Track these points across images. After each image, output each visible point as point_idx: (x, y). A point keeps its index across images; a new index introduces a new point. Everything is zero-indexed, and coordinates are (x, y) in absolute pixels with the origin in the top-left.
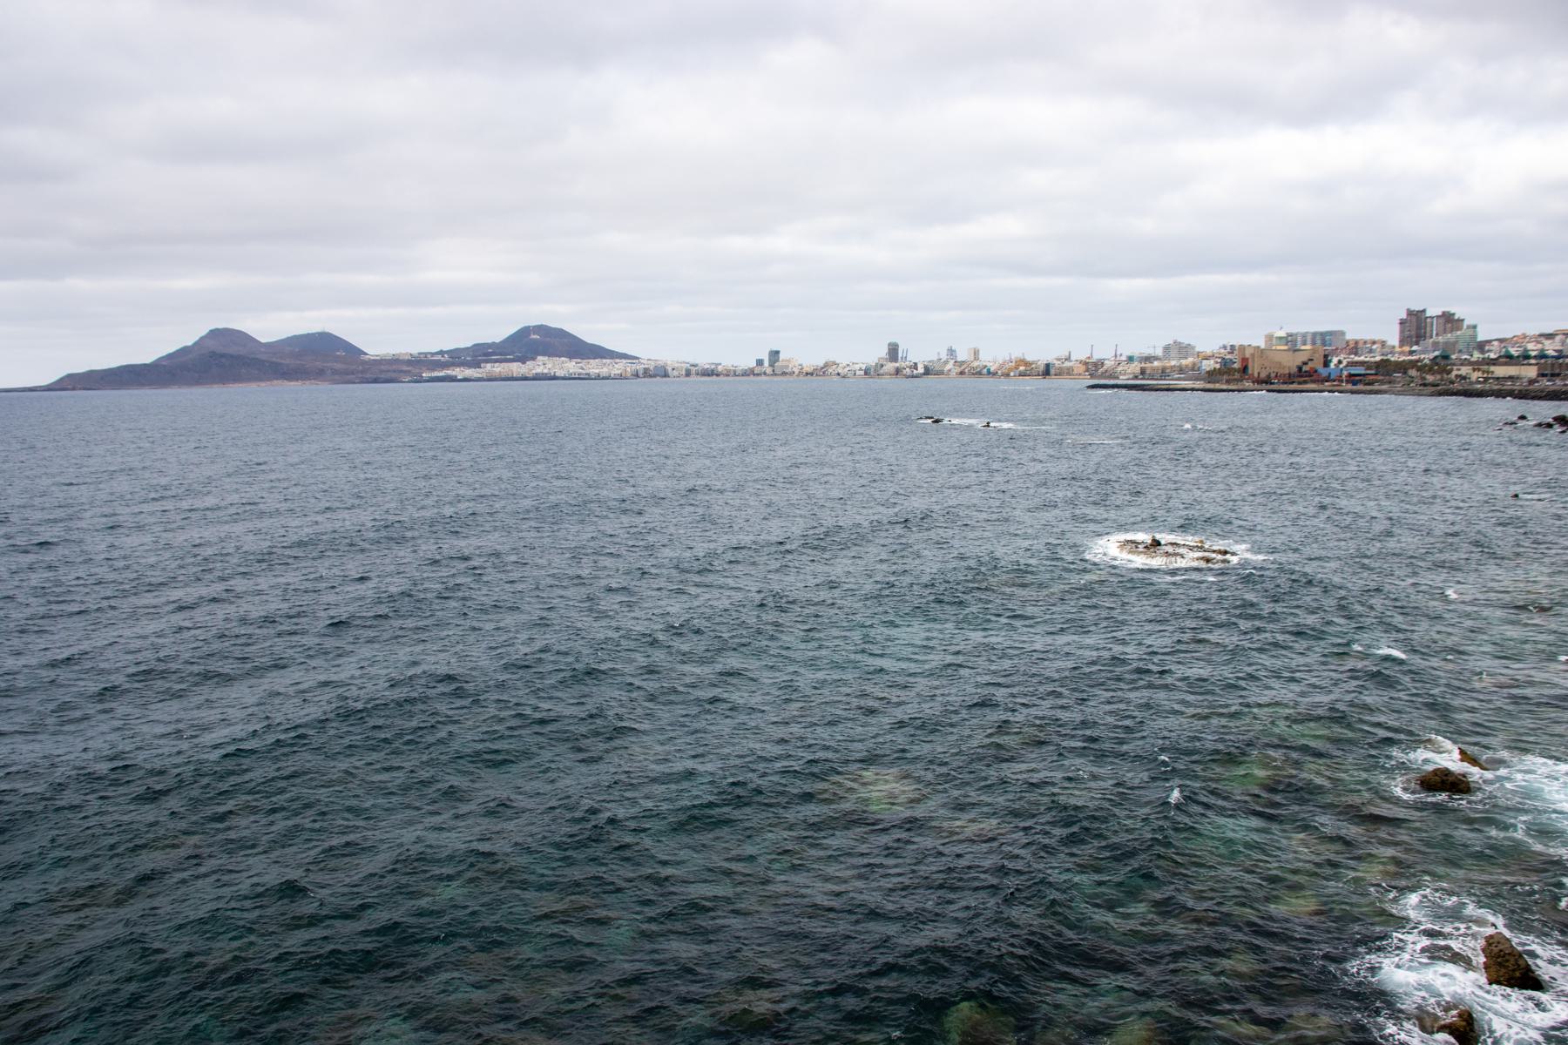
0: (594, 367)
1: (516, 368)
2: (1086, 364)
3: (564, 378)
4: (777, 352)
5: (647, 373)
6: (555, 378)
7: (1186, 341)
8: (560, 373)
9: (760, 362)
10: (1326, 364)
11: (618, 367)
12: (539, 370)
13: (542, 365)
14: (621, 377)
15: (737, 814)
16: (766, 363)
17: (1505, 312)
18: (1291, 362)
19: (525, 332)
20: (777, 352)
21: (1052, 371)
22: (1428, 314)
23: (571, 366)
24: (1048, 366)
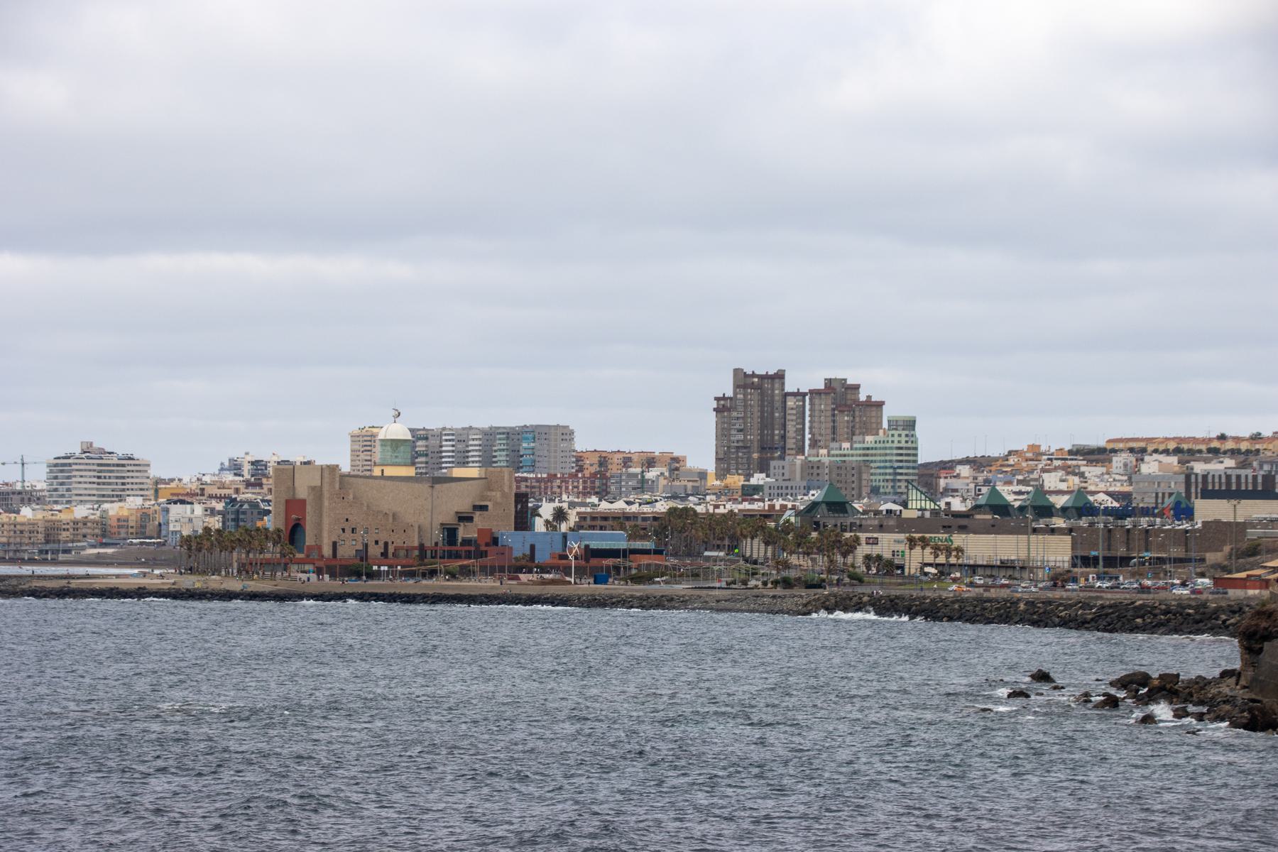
10: (523, 520)
18: (425, 514)
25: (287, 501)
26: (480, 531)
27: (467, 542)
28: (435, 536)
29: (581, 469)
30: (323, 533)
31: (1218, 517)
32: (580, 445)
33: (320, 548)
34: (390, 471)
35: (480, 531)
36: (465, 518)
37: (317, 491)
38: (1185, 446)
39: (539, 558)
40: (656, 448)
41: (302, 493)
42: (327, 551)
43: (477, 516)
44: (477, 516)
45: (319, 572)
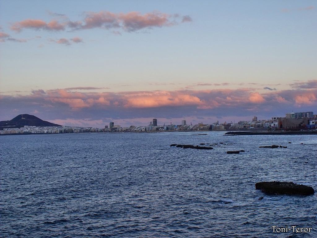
0: (45, 130)
1: (17, 130)
2: (224, 125)
3: (34, 134)
4: (113, 123)
5: (66, 132)
6: (31, 133)
7: (227, 123)
8: (33, 132)
9: (106, 127)
10: (309, 123)
11: (55, 129)
12: (26, 130)
13: (26, 129)
14: (55, 133)
15: (153, 220)
16: (109, 127)
17: (303, 103)
18: (298, 122)
19: (20, 116)
20: (113, 123)
21: (213, 128)
22: (314, 114)
23: (37, 129)
24: (211, 126)
25: (280, 122)
26: (304, 125)
27: (302, 126)
28: (298, 126)
29: (314, 117)
30: (285, 126)
31: (43, 89)
32: (314, 114)
33: (284, 127)
34: (292, 118)
35: (304, 125)
36: (302, 123)
37: (284, 121)
38: (162, 122)
39: (311, 128)
40: (221, 123)
41: (282, 121)
42: (285, 128)
43: (303, 123)
44: (303, 123)
45: (285, 130)
